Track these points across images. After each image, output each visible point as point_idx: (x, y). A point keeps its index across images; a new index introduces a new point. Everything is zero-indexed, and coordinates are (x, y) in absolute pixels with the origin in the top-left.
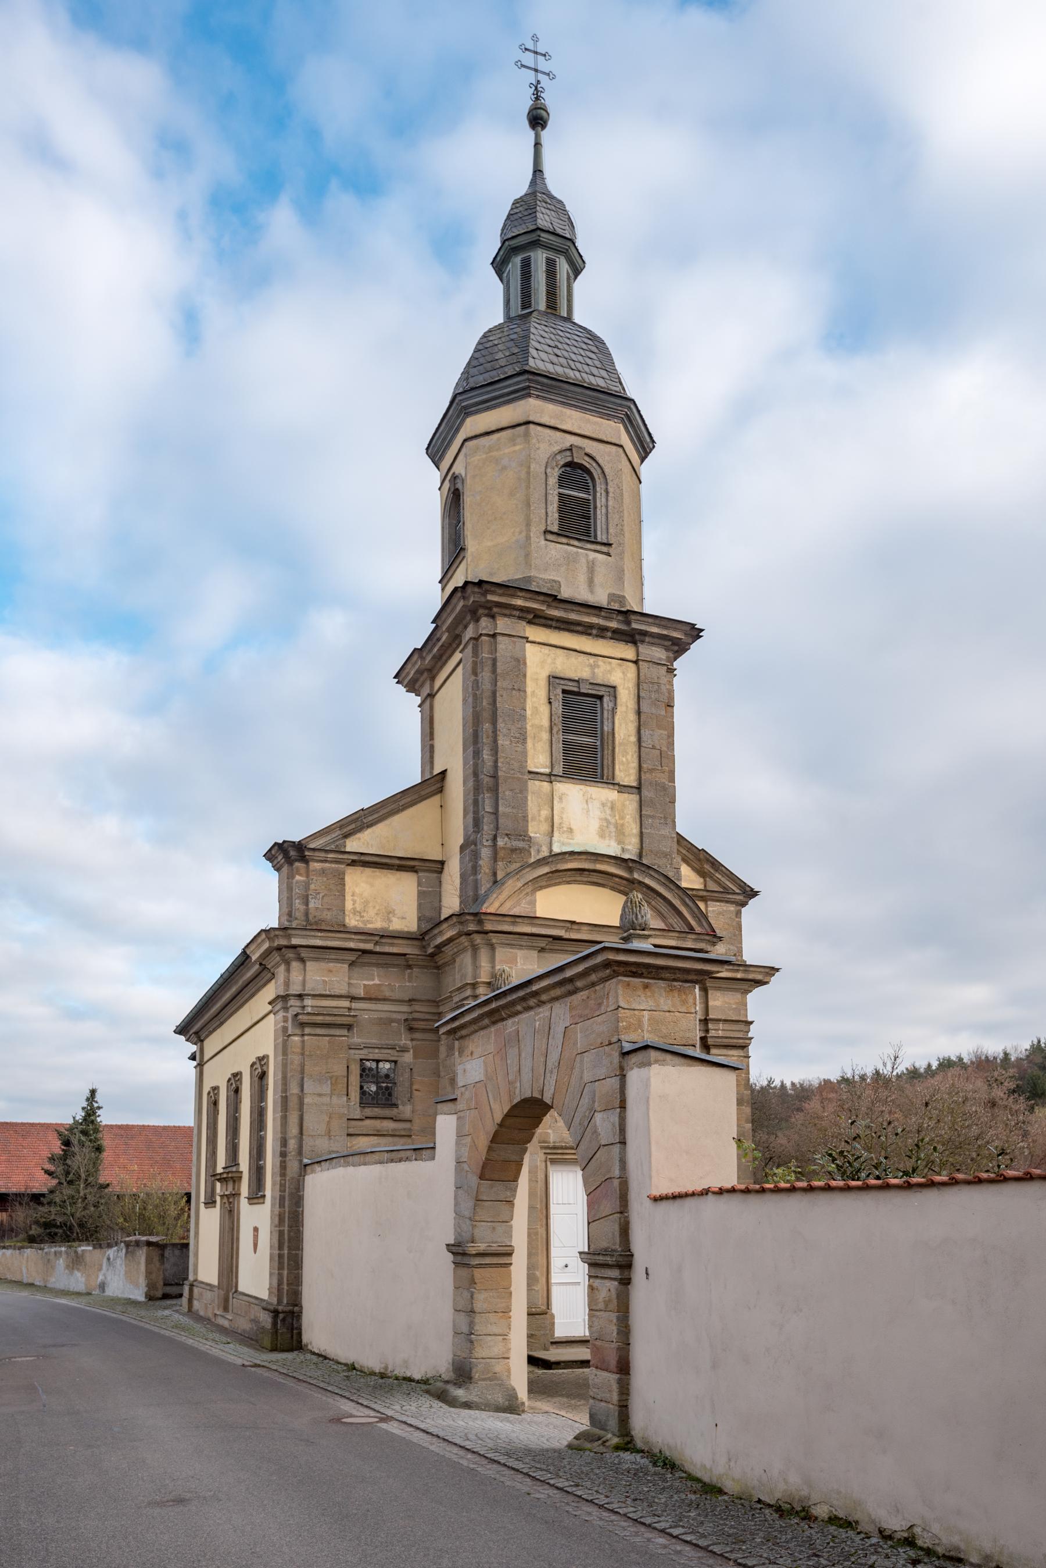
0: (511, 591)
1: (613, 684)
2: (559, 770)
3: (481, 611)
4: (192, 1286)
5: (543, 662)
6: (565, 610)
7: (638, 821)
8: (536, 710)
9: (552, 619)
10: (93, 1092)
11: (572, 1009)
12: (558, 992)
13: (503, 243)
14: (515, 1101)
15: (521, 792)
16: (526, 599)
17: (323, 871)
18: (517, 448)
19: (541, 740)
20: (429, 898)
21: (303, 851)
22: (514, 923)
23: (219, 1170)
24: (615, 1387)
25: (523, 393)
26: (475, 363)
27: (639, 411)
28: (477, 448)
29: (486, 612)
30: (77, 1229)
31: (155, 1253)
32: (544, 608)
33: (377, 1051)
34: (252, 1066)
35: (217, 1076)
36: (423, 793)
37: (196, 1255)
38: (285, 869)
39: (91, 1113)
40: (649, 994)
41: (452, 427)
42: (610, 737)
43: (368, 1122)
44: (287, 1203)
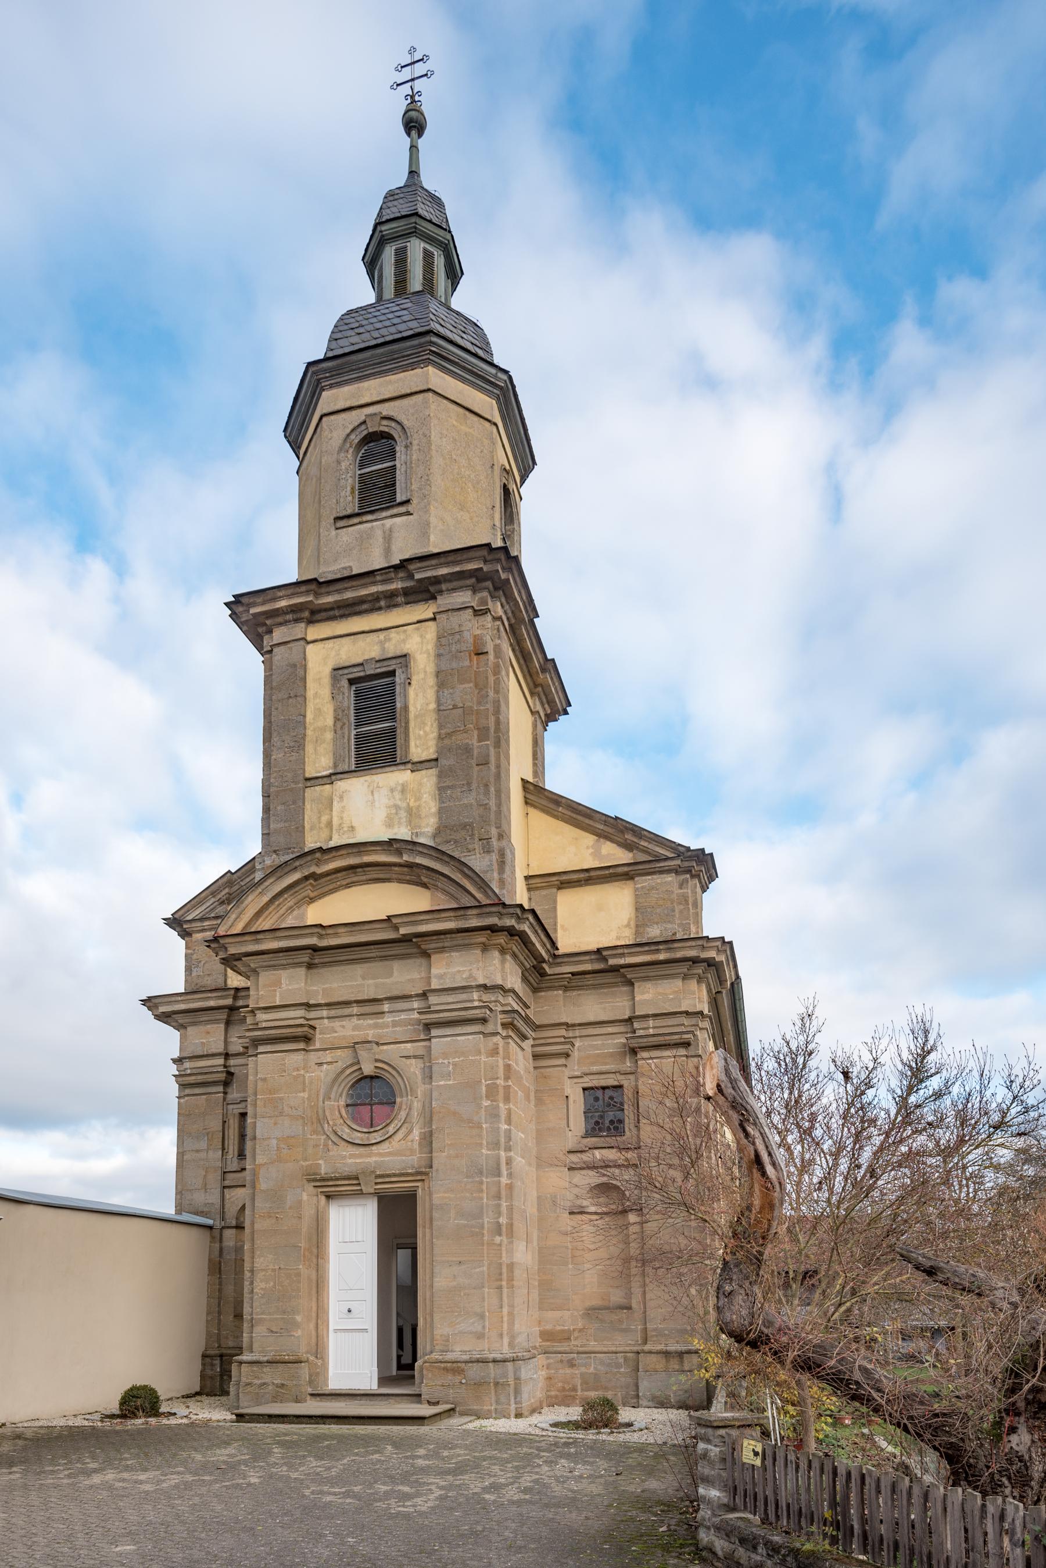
8: (319, 712)
32: (310, 598)
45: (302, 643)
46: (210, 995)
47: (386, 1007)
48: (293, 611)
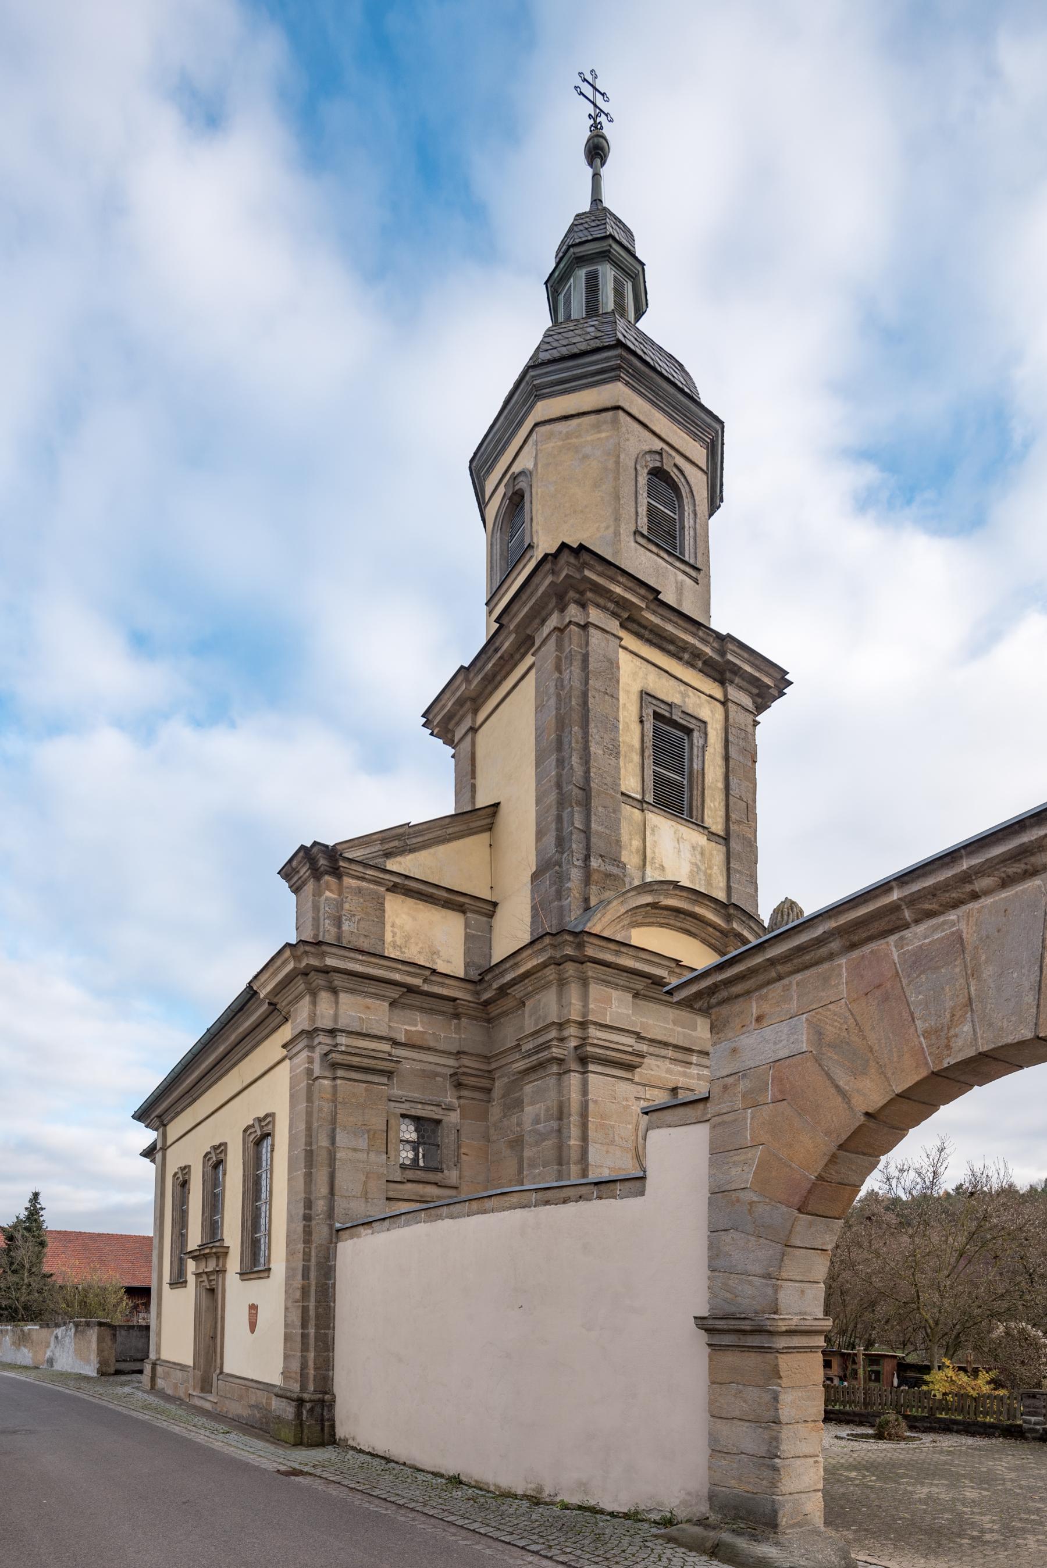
0: (611, 572)
1: (705, 719)
3: (572, 594)
4: (154, 1365)
5: (635, 674)
6: (663, 618)
7: (725, 874)
9: (645, 627)
10: (36, 1195)
15: (614, 811)
16: (627, 588)
17: (359, 891)
18: (603, 435)
19: (631, 761)
20: (478, 941)
21: (337, 861)
22: (617, 953)
27: (723, 444)
28: (551, 435)
29: (577, 596)
30: (21, 1311)
31: (107, 1333)
33: (420, 1106)
36: (473, 825)
37: (159, 1334)
38: (310, 886)
39: (34, 1212)
41: (513, 422)
42: (700, 777)
43: (409, 1186)
44: (313, 1275)
46: (400, 967)
47: (694, 1059)
48: (617, 603)
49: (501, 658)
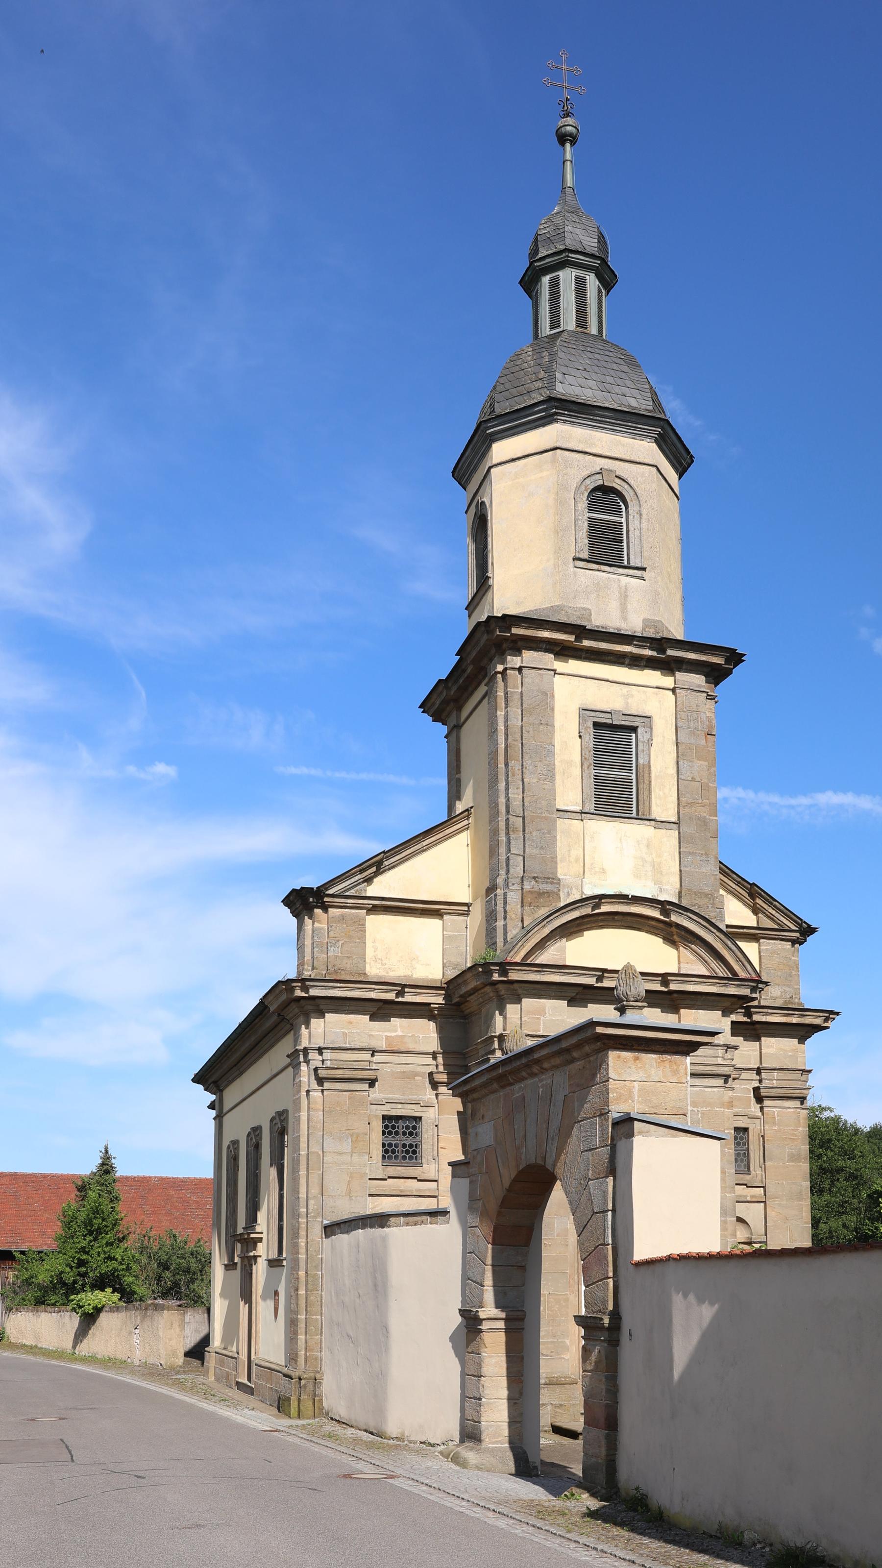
2: (590, 807)
3: (505, 646)
11: (570, 1077)
12: (557, 1061)
13: (531, 263)
14: (521, 1167)
15: (549, 832)
17: (343, 918)
18: (545, 474)
23: (240, 1230)
24: (603, 1442)
25: (547, 420)
26: (500, 388)
33: (400, 1106)
34: (271, 1121)
35: (237, 1129)
39: (106, 1167)
40: (639, 1065)
45: (553, 673)
49: (468, 677)
